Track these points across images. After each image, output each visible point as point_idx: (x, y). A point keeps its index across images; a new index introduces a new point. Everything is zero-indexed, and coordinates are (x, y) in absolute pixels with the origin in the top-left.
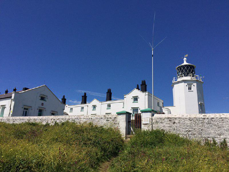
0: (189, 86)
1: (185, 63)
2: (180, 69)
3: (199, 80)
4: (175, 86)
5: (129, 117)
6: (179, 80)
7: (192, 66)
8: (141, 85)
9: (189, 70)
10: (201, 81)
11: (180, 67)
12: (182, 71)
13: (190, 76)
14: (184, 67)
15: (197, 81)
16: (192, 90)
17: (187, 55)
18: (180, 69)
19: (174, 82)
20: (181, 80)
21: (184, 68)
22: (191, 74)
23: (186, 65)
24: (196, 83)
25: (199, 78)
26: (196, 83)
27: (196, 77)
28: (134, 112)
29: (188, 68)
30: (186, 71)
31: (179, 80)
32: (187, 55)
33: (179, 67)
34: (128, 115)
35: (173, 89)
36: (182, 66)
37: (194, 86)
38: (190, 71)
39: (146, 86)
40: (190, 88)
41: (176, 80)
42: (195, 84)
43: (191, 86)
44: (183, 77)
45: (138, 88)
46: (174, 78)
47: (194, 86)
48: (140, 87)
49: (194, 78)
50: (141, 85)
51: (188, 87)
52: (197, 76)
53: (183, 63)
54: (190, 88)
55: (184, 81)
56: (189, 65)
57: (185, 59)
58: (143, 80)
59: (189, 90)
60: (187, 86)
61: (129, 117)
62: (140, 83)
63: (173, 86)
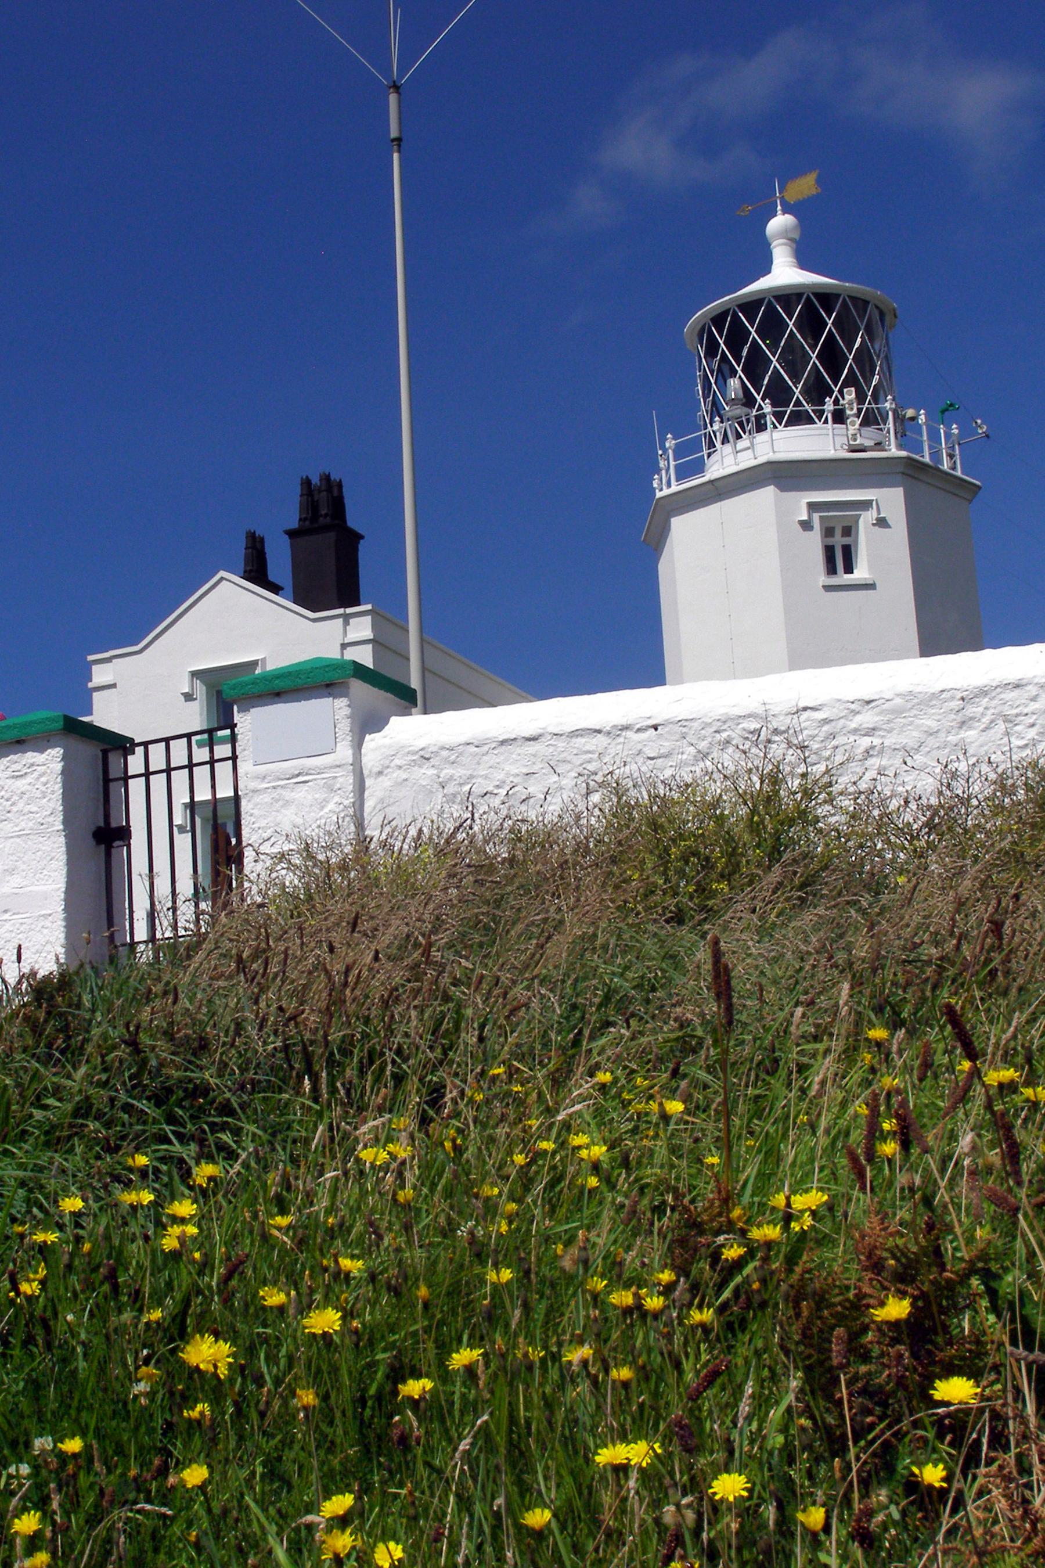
0: (828, 532)
1: (785, 272)
2: (737, 338)
3: (936, 455)
4: (683, 527)
5: (107, 781)
6: (724, 462)
7: (861, 303)
8: (291, 534)
9: (808, 353)
10: (959, 473)
11: (729, 326)
12: (755, 367)
13: (839, 417)
14: (771, 310)
15: (913, 473)
16: (861, 573)
17: (805, 186)
18: (737, 338)
19: (675, 488)
20: (746, 461)
21: (772, 327)
22: (850, 394)
23: (788, 297)
24: (900, 491)
25: (934, 437)
26: (900, 491)
27: (905, 428)
28: (537, 1173)
29: (812, 325)
30: (794, 362)
31: (724, 462)
32: (805, 186)
33: (718, 320)
34: (90, 751)
35: (662, 567)
36: (750, 307)
37: (882, 523)
38: (832, 358)
39: (350, 540)
40: (839, 557)
41: (699, 467)
42: (891, 500)
43: (847, 531)
44: (761, 427)
45: (257, 572)
46: (670, 443)
47: (882, 523)
48: (280, 561)
49: (879, 446)
50: (291, 534)
51: (814, 543)
52: (910, 413)
53: (765, 267)
54: (839, 557)
55: (786, 475)
56: (826, 298)
57: (780, 223)
58: (315, 480)
59: (831, 570)
60: (806, 525)
61: (107, 781)
62: (279, 516)
63: (664, 531)
